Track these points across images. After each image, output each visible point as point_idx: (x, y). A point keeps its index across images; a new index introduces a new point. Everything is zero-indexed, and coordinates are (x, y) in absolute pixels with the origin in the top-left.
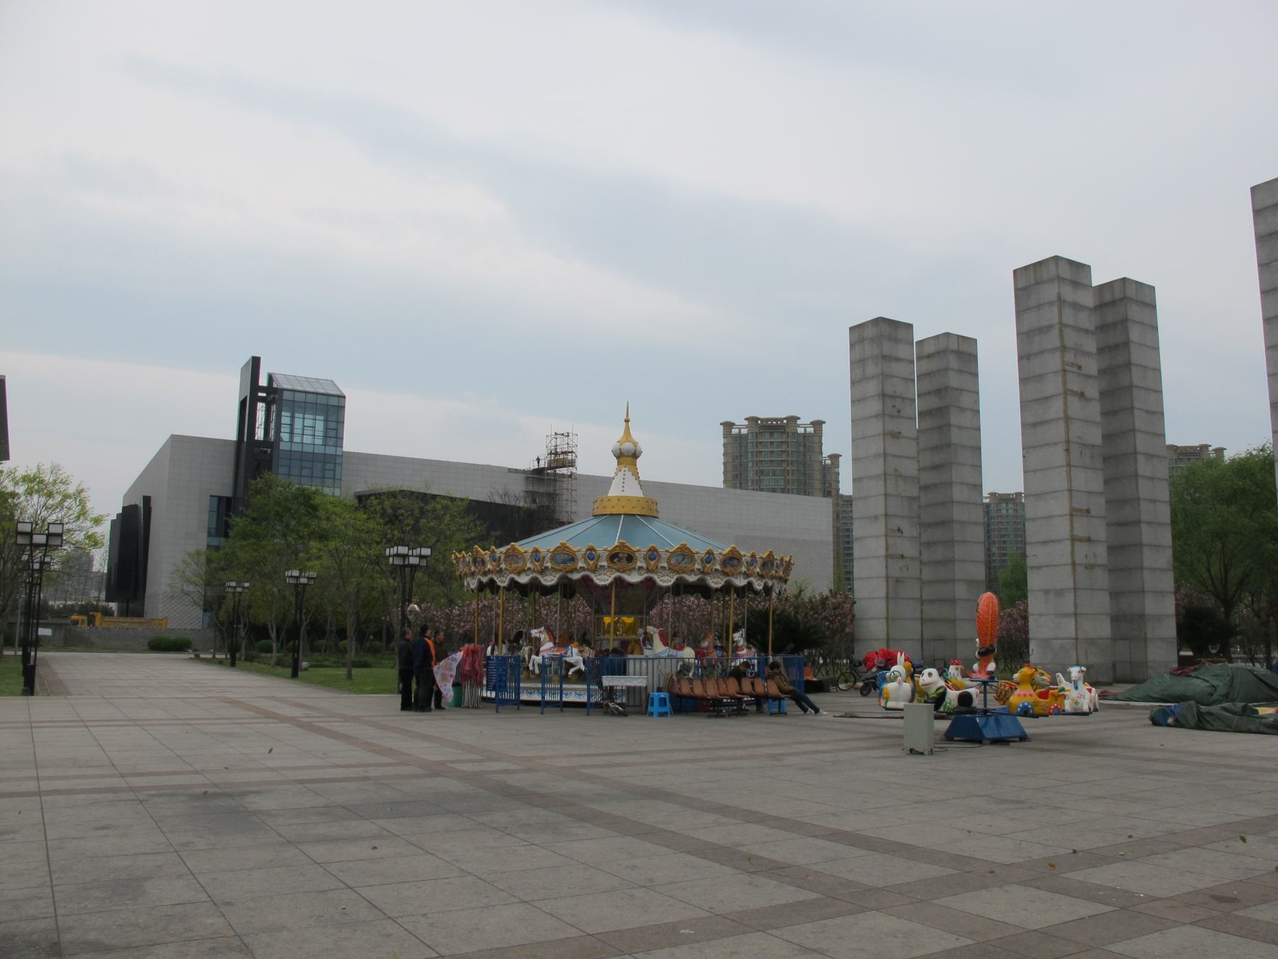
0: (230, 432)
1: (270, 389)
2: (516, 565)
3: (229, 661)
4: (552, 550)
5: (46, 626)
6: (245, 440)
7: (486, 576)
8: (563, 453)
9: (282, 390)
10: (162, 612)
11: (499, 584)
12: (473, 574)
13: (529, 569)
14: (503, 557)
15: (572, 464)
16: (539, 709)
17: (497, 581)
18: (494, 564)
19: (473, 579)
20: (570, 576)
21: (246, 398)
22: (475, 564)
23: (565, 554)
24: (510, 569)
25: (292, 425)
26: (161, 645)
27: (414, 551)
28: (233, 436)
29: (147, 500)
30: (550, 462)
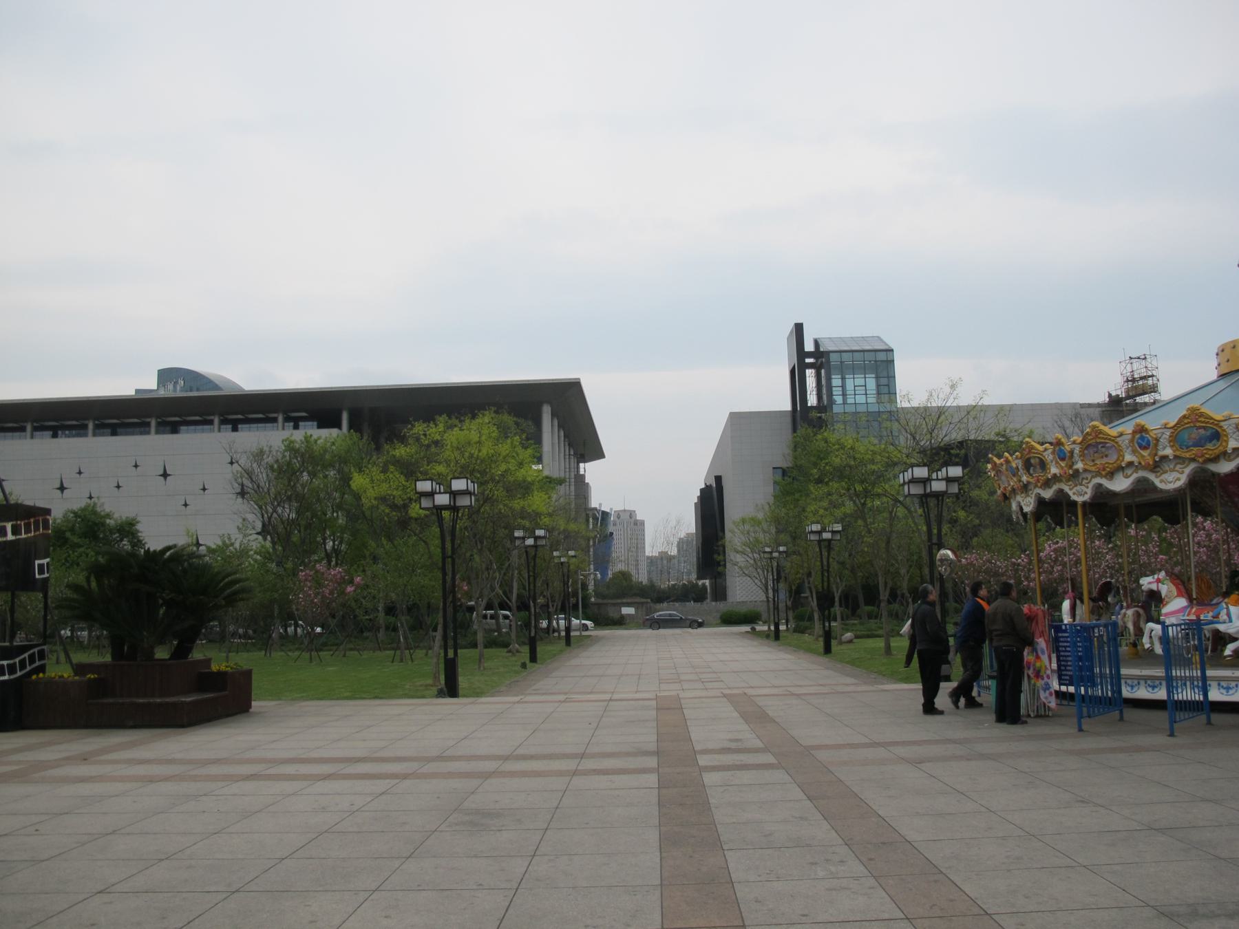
0: (782, 402)
1: (818, 353)
2: (1104, 461)
3: (772, 635)
4: (1172, 424)
5: (628, 605)
6: (799, 409)
7: (1050, 488)
8: (1142, 378)
9: (828, 353)
10: (739, 590)
11: (1074, 498)
12: (1025, 488)
13: (1130, 464)
14: (1077, 451)
15: (1154, 389)
16: (1161, 717)
17: (1070, 493)
18: (1063, 464)
19: (1028, 496)
20: (1213, 467)
21: (794, 366)
22: (1028, 470)
23: (1200, 428)
24: (1093, 469)
25: (843, 387)
26: (730, 619)
27: (939, 473)
28: (787, 406)
29: (718, 479)
30: (1128, 391)
